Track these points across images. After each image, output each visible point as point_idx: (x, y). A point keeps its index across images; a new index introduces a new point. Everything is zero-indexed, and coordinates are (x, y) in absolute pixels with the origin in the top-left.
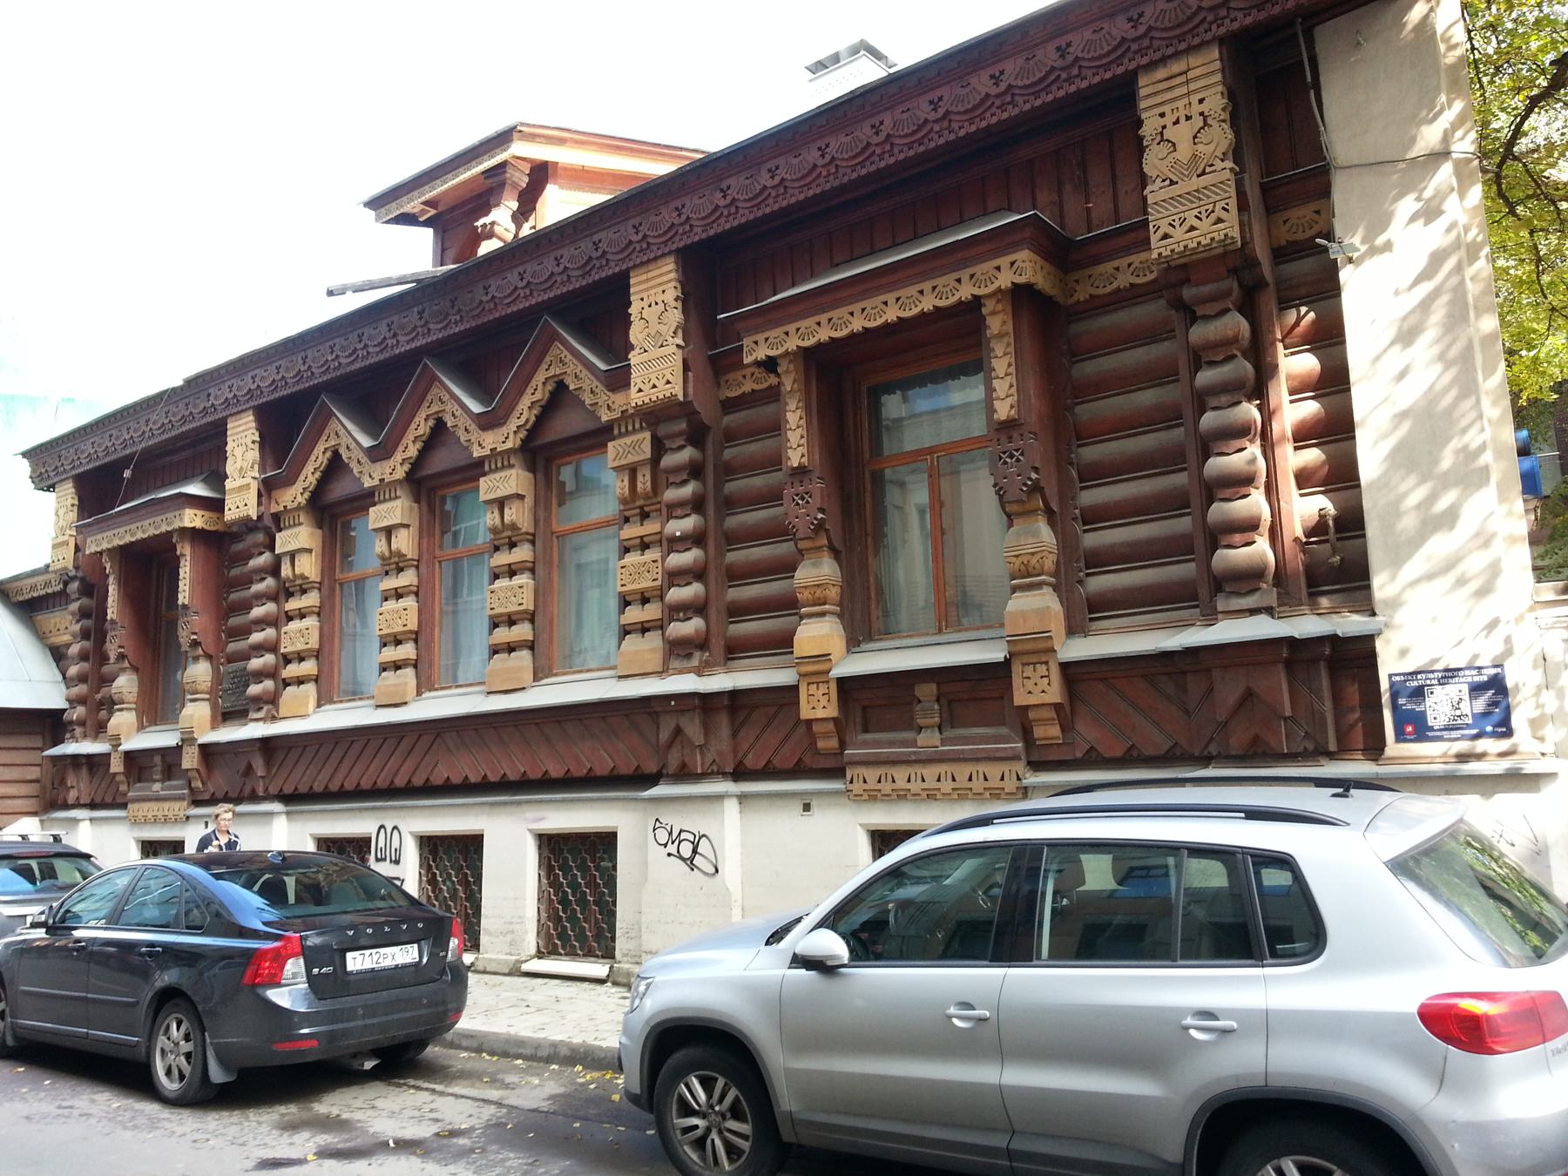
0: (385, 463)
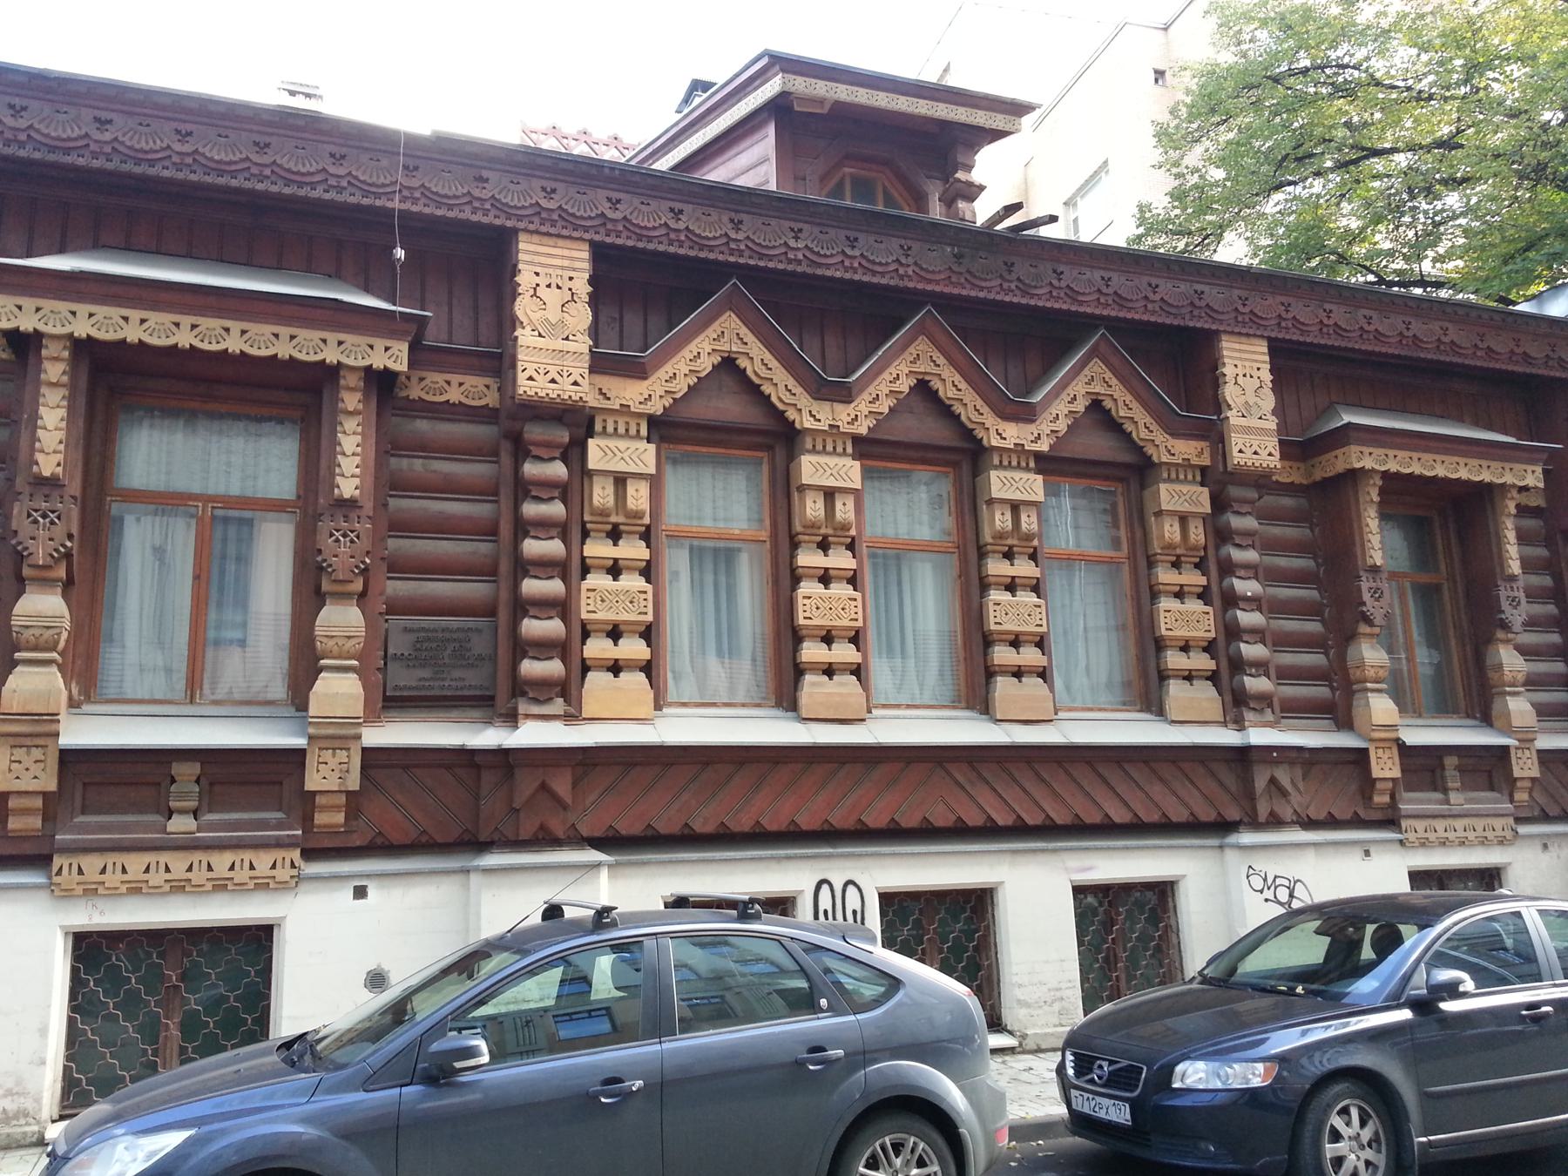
0: (839, 407)
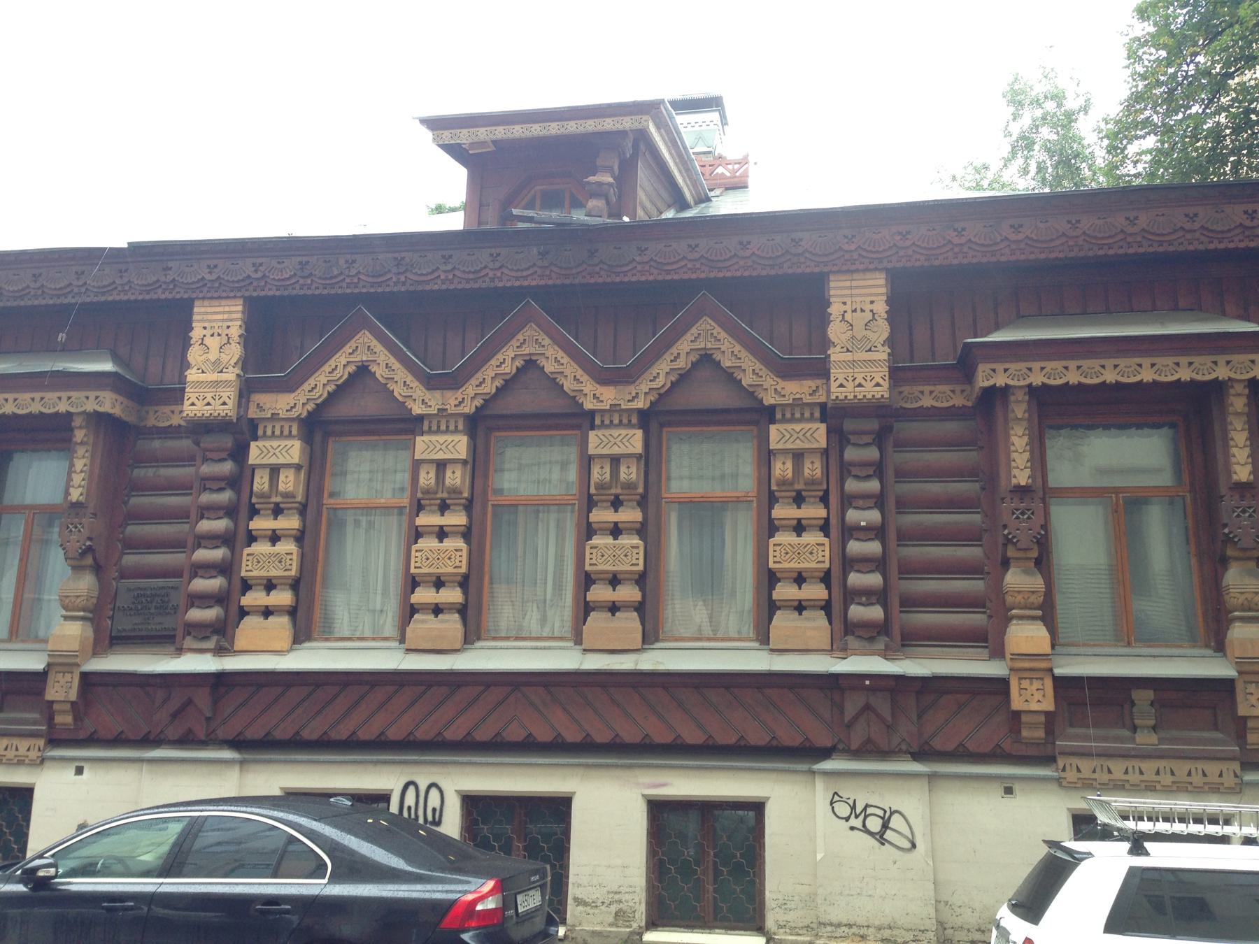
0: (449, 394)
